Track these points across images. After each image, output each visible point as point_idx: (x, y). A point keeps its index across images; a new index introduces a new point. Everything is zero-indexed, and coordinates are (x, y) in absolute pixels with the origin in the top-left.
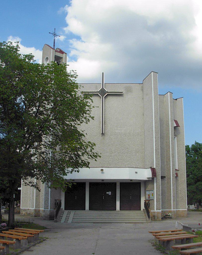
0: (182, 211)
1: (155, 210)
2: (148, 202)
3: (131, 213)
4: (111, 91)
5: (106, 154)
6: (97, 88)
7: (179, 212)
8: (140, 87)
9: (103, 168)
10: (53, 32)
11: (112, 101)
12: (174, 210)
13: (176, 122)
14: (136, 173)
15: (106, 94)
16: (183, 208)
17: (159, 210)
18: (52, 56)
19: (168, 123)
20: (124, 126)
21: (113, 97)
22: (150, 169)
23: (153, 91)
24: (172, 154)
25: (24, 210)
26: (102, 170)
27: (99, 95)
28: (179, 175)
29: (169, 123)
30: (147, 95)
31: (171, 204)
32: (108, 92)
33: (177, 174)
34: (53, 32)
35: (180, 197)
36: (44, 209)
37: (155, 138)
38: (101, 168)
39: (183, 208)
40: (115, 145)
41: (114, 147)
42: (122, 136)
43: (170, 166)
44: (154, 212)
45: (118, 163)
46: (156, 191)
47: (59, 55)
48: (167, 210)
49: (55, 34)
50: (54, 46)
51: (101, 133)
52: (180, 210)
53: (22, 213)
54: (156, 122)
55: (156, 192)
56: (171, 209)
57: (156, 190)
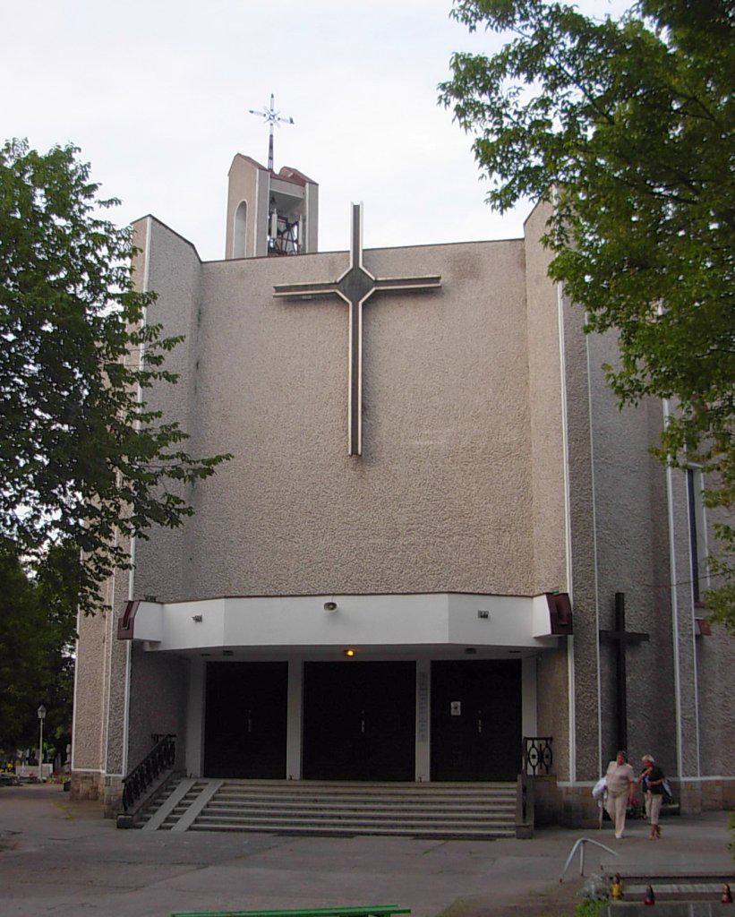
2: (543, 747)
4: (389, 278)
5: (371, 541)
6: (333, 271)
8: (513, 255)
9: (336, 600)
10: (265, 108)
11: (400, 322)
12: (692, 779)
14: (484, 616)
18: (257, 195)
20: (448, 419)
21: (403, 303)
22: (545, 597)
25: (86, 777)
27: (342, 299)
30: (536, 281)
32: (377, 283)
34: (265, 108)
36: (108, 772)
38: (329, 599)
41: (404, 509)
42: (440, 465)
45: (421, 576)
46: (577, 696)
47: (291, 190)
49: (273, 116)
50: (271, 158)
51: (350, 453)
53: (76, 788)
54: (574, 395)
55: (577, 701)
57: (576, 690)
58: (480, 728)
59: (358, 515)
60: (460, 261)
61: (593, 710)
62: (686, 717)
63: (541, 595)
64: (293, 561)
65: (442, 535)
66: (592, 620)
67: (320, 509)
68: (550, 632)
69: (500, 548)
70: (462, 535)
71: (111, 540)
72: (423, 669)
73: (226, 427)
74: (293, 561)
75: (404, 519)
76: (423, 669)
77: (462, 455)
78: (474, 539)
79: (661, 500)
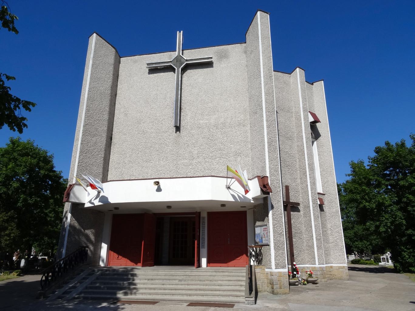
0: (337, 268)
1: (274, 270)
3: (218, 274)
5: (182, 161)
7: (331, 269)
9: (160, 181)
13: (314, 115)
15: (185, 63)
16: (339, 261)
17: (281, 268)
19: (299, 114)
22: (256, 179)
23: (260, 40)
24: (308, 164)
26: (157, 183)
28: (326, 203)
29: (300, 114)
31: (314, 255)
33: (321, 200)
35: (331, 241)
37: (267, 121)
39: (339, 261)
40: (199, 145)
43: (307, 185)
44: (272, 274)
46: (274, 225)
48: (307, 265)
52: (335, 266)
55: (274, 228)
56: (315, 264)
58: (229, 242)
59: (177, 151)
60: (220, 52)
61: (281, 233)
62: (317, 238)
63: (253, 178)
64: (150, 170)
65: (212, 158)
66: (279, 190)
67: (162, 149)
68: (260, 194)
69: (236, 163)
70: (220, 158)
71: (21, 131)
72: (204, 215)
73: (126, 118)
74: (150, 170)
75: (196, 152)
76: (204, 215)
77: (220, 126)
78: (225, 159)
79: (302, 150)
